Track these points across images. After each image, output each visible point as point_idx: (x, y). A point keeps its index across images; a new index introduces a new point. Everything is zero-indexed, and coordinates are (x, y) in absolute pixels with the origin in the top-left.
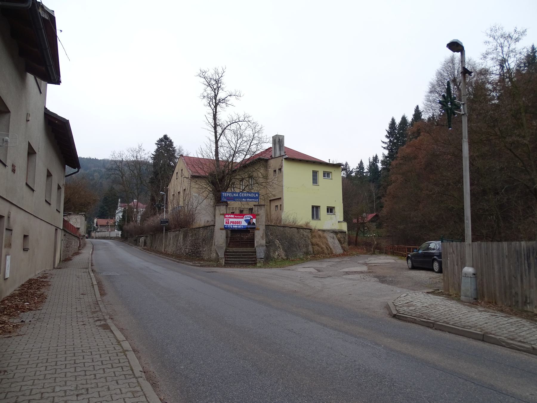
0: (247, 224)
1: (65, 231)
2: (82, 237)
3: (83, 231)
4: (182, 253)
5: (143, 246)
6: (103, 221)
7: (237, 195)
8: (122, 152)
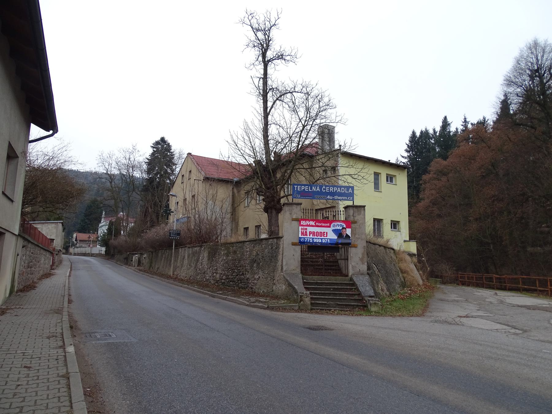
0: (336, 237)
1: (25, 239)
2: (57, 253)
3: (58, 244)
4: (207, 280)
5: (136, 266)
6: (83, 236)
7: (318, 189)
8: (112, 153)
